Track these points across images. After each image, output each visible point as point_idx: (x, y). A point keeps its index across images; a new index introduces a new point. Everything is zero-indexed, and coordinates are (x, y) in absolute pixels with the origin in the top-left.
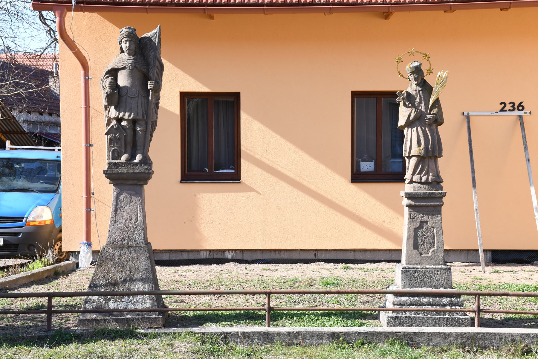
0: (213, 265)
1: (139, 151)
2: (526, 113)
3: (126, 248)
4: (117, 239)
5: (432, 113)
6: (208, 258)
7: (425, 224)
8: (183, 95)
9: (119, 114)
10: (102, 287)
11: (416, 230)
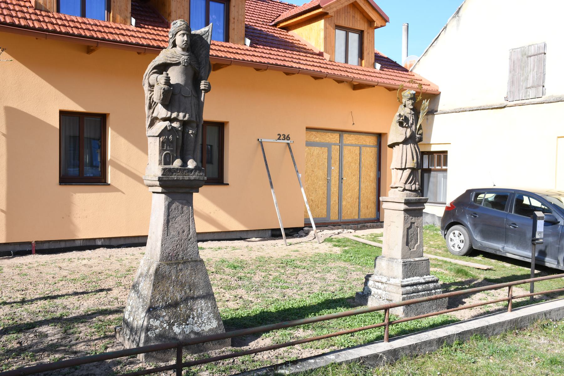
0: (86, 251)
1: (190, 156)
2: (291, 142)
3: (182, 263)
4: (170, 255)
5: (419, 133)
6: (82, 245)
7: (413, 224)
8: (63, 114)
9: (171, 115)
10: (163, 310)
11: (408, 229)
